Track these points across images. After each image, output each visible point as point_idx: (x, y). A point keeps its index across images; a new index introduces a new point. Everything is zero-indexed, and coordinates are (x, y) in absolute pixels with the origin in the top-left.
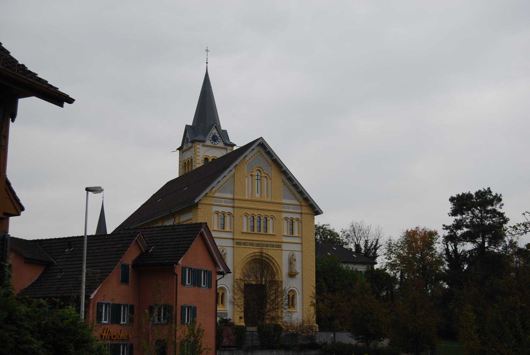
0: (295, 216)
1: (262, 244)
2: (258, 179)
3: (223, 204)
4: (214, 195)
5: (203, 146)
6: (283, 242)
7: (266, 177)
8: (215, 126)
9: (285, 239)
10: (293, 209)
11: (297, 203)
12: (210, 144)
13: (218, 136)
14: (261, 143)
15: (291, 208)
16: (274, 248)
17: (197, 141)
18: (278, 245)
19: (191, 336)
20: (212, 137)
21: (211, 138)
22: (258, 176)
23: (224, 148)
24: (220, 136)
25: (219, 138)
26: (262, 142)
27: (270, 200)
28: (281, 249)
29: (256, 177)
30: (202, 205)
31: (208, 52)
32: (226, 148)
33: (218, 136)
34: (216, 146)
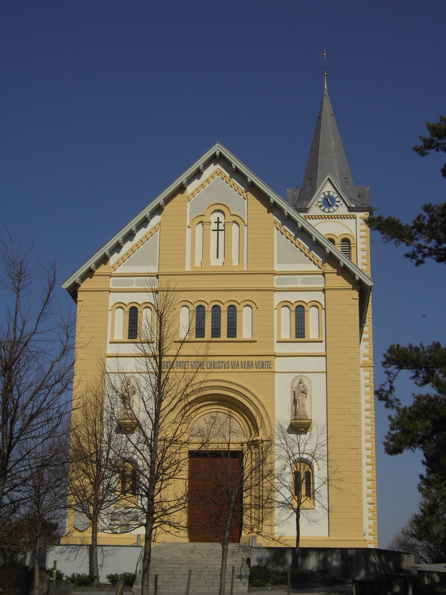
0: (306, 297)
2: (218, 230)
3: (134, 287)
4: (115, 272)
6: (276, 356)
7: (234, 222)
8: (327, 178)
9: (279, 349)
10: (303, 281)
11: (316, 268)
12: (319, 212)
13: (335, 196)
14: (218, 154)
15: (299, 280)
20: (323, 200)
21: (320, 202)
22: (218, 222)
25: (322, 196)
26: (220, 153)
27: (245, 269)
28: (269, 370)
29: (214, 226)
32: (353, 215)
33: (335, 196)
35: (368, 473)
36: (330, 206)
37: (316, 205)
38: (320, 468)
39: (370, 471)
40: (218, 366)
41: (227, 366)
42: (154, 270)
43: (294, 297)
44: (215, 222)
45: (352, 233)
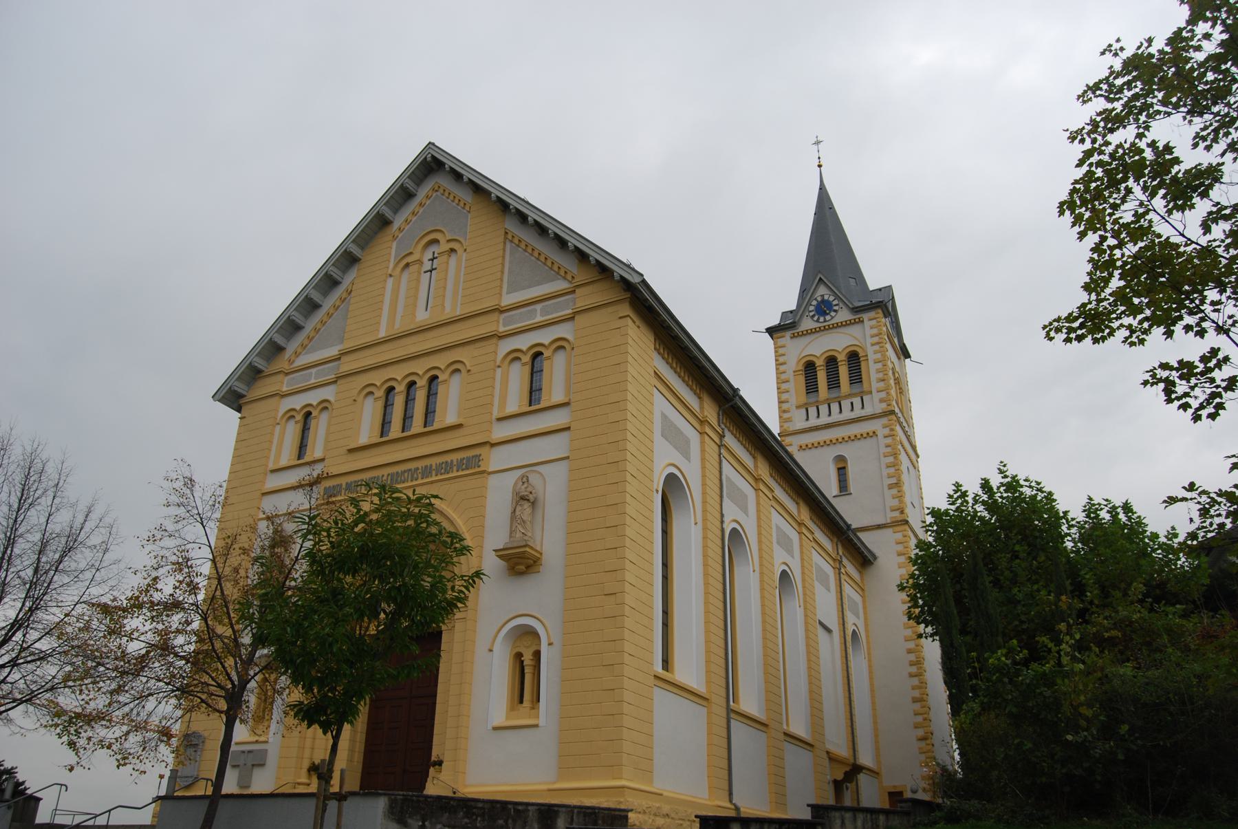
1: (410, 470)
5: (793, 337)
13: (831, 298)
16: (451, 475)
17: (776, 331)
19: (470, 823)
25: (814, 303)
26: (433, 157)
28: (477, 470)
30: (254, 405)
35: (913, 689)
38: (552, 641)
41: (415, 476)
42: (333, 351)
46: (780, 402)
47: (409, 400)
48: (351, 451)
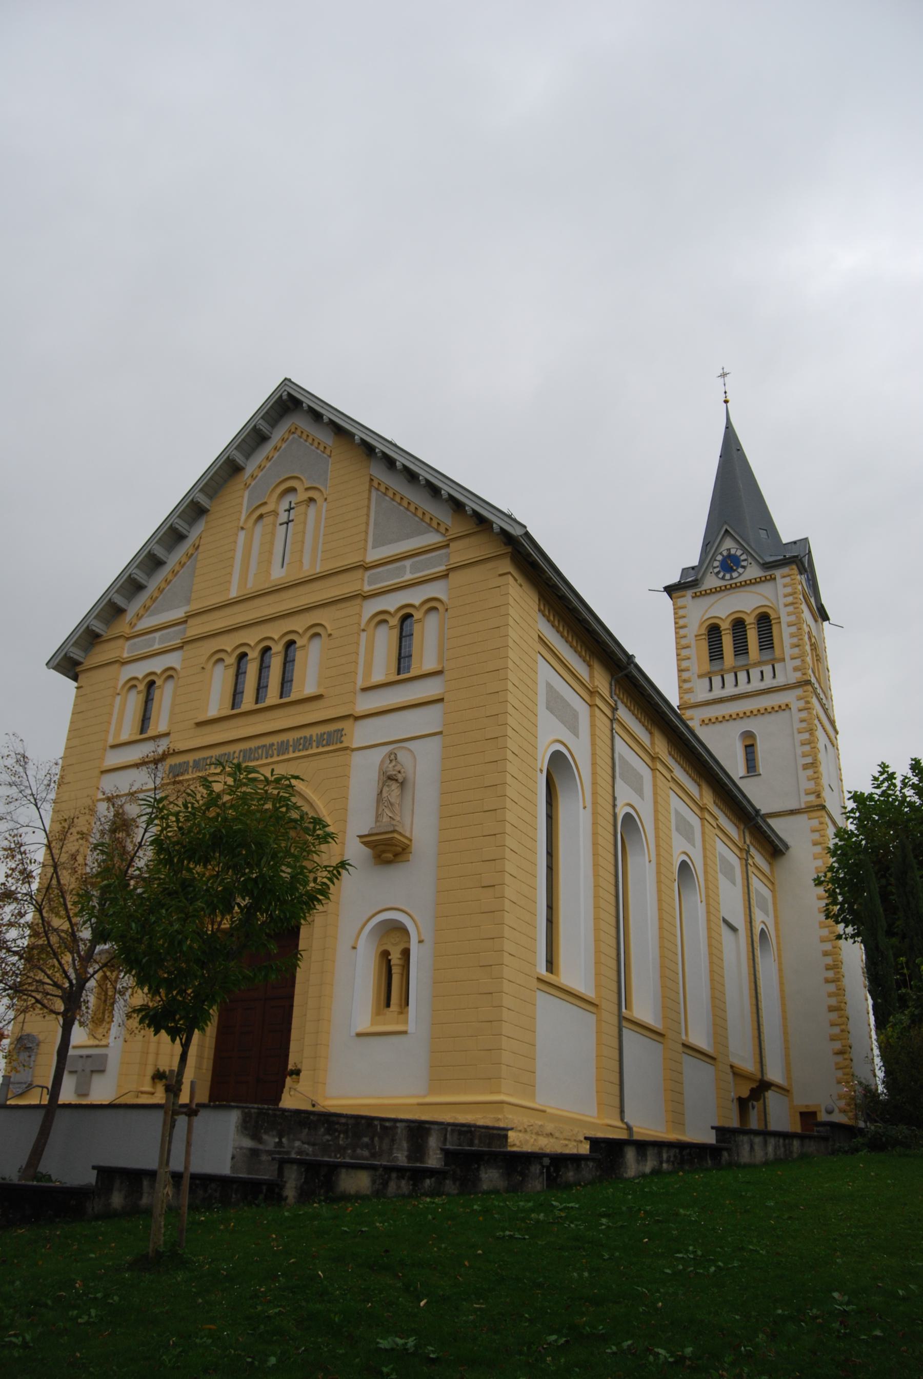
5: (695, 596)
8: (724, 530)
10: (414, 569)
13: (739, 553)
16: (310, 752)
18: (329, 734)
21: (717, 567)
23: (765, 577)
24: (745, 551)
25: (719, 558)
26: (289, 395)
28: (339, 746)
31: (727, 378)
32: (771, 576)
34: (736, 584)
36: (731, 570)
37: (711, 573)
38: (423, 938)
39: (833, 993)
40: (256, 755)
43: (391, 603)
44: (285, 511)
45: (772, 603)
46: (680, 671)
47: (718, 637)
48: (199, 724)
